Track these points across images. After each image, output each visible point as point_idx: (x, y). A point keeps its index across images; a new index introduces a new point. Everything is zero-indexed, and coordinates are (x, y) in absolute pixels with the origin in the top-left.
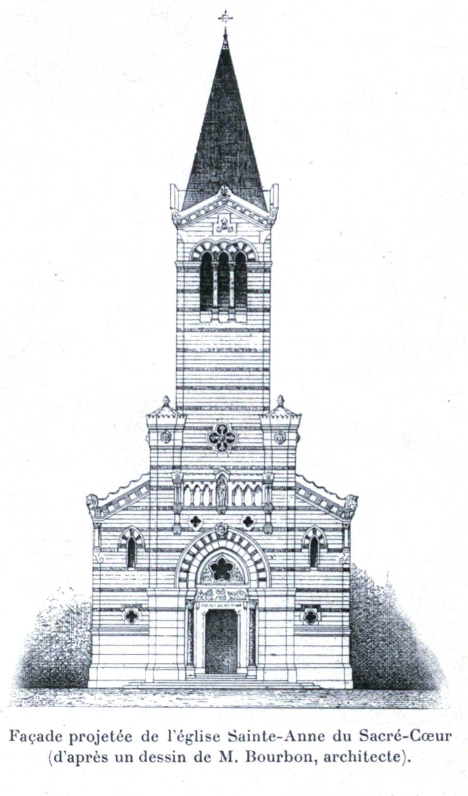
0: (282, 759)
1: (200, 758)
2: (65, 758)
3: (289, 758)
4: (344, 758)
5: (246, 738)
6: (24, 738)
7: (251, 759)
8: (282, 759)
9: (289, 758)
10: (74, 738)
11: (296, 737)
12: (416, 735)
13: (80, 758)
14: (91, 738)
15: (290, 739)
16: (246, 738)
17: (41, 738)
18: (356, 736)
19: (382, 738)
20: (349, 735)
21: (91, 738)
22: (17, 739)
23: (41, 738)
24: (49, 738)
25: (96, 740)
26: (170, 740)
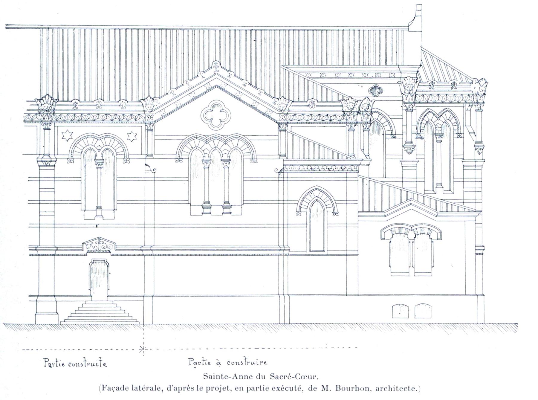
0: (354, 390)
1: (312, 389)
2: (172, 388)
3: (357, 389)
4: (386, 389)
5: (213, 377)
6: (109, 389)
7: (338, 389)
8: (354, 390)
9: (357, 389)
10: (208, 389)
11: (238, 377)
12: (298, 377)
13: (180, 389)
14: (217, 389)
15: (235, 378)
16: (213, 377)
17: (118, 389)
18: (268, 377)
19: (282, 377)
20: (30, 296)
21: (217, 389)
22: (106, 389)
23: (118, 389)
24: (122, 389)
25: (219, 390)
26: (8, 27)
